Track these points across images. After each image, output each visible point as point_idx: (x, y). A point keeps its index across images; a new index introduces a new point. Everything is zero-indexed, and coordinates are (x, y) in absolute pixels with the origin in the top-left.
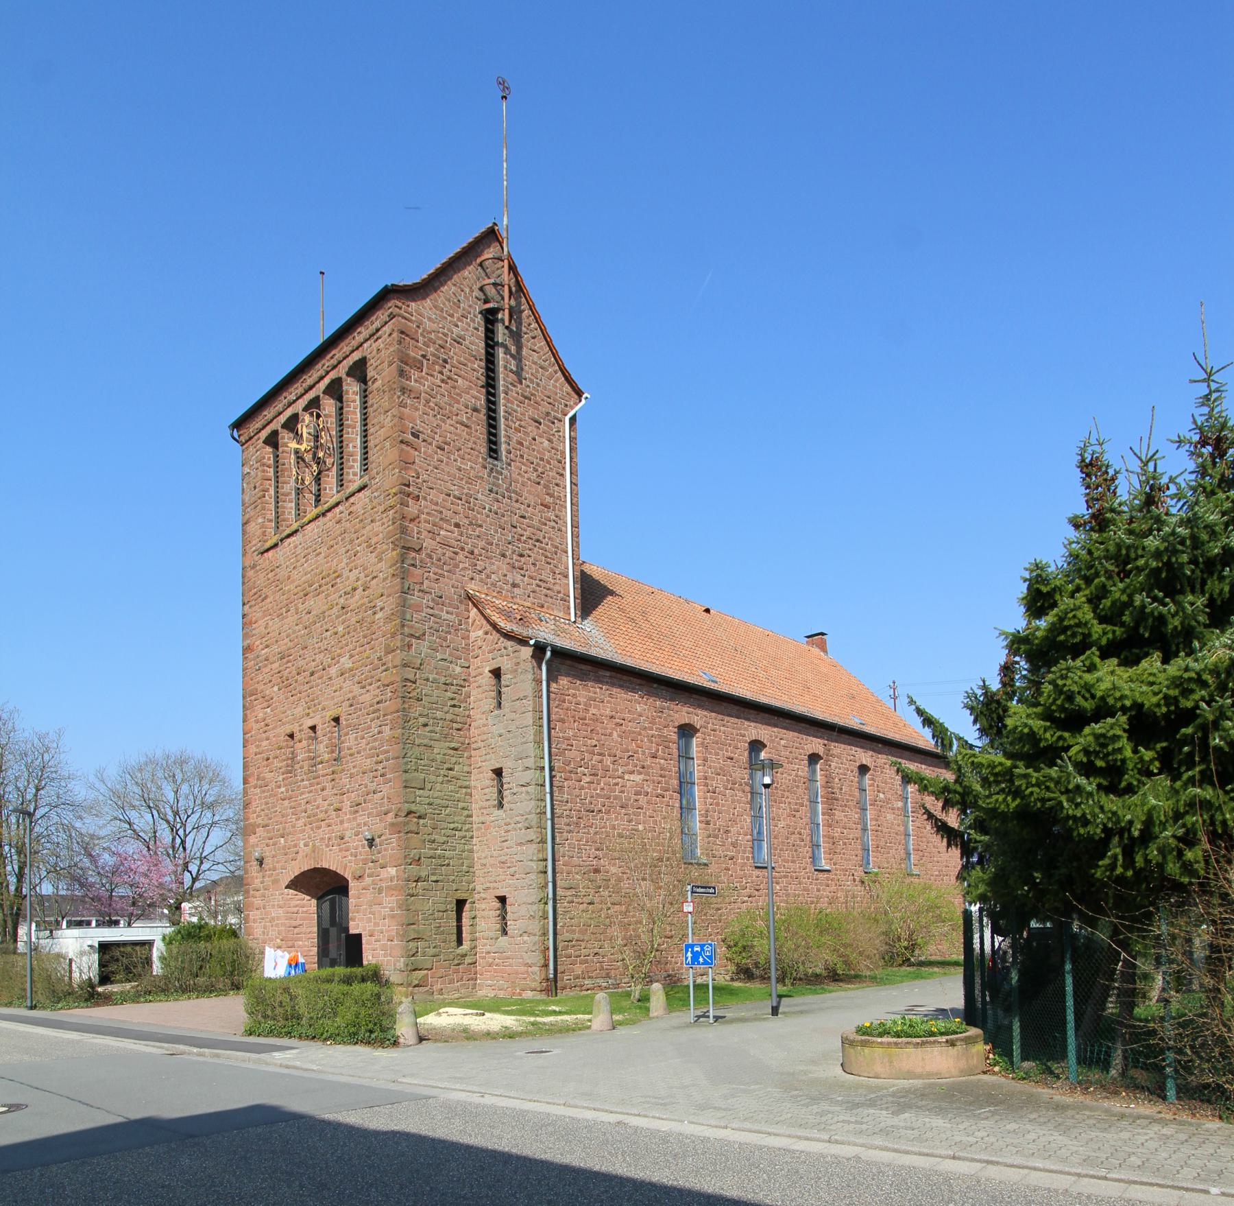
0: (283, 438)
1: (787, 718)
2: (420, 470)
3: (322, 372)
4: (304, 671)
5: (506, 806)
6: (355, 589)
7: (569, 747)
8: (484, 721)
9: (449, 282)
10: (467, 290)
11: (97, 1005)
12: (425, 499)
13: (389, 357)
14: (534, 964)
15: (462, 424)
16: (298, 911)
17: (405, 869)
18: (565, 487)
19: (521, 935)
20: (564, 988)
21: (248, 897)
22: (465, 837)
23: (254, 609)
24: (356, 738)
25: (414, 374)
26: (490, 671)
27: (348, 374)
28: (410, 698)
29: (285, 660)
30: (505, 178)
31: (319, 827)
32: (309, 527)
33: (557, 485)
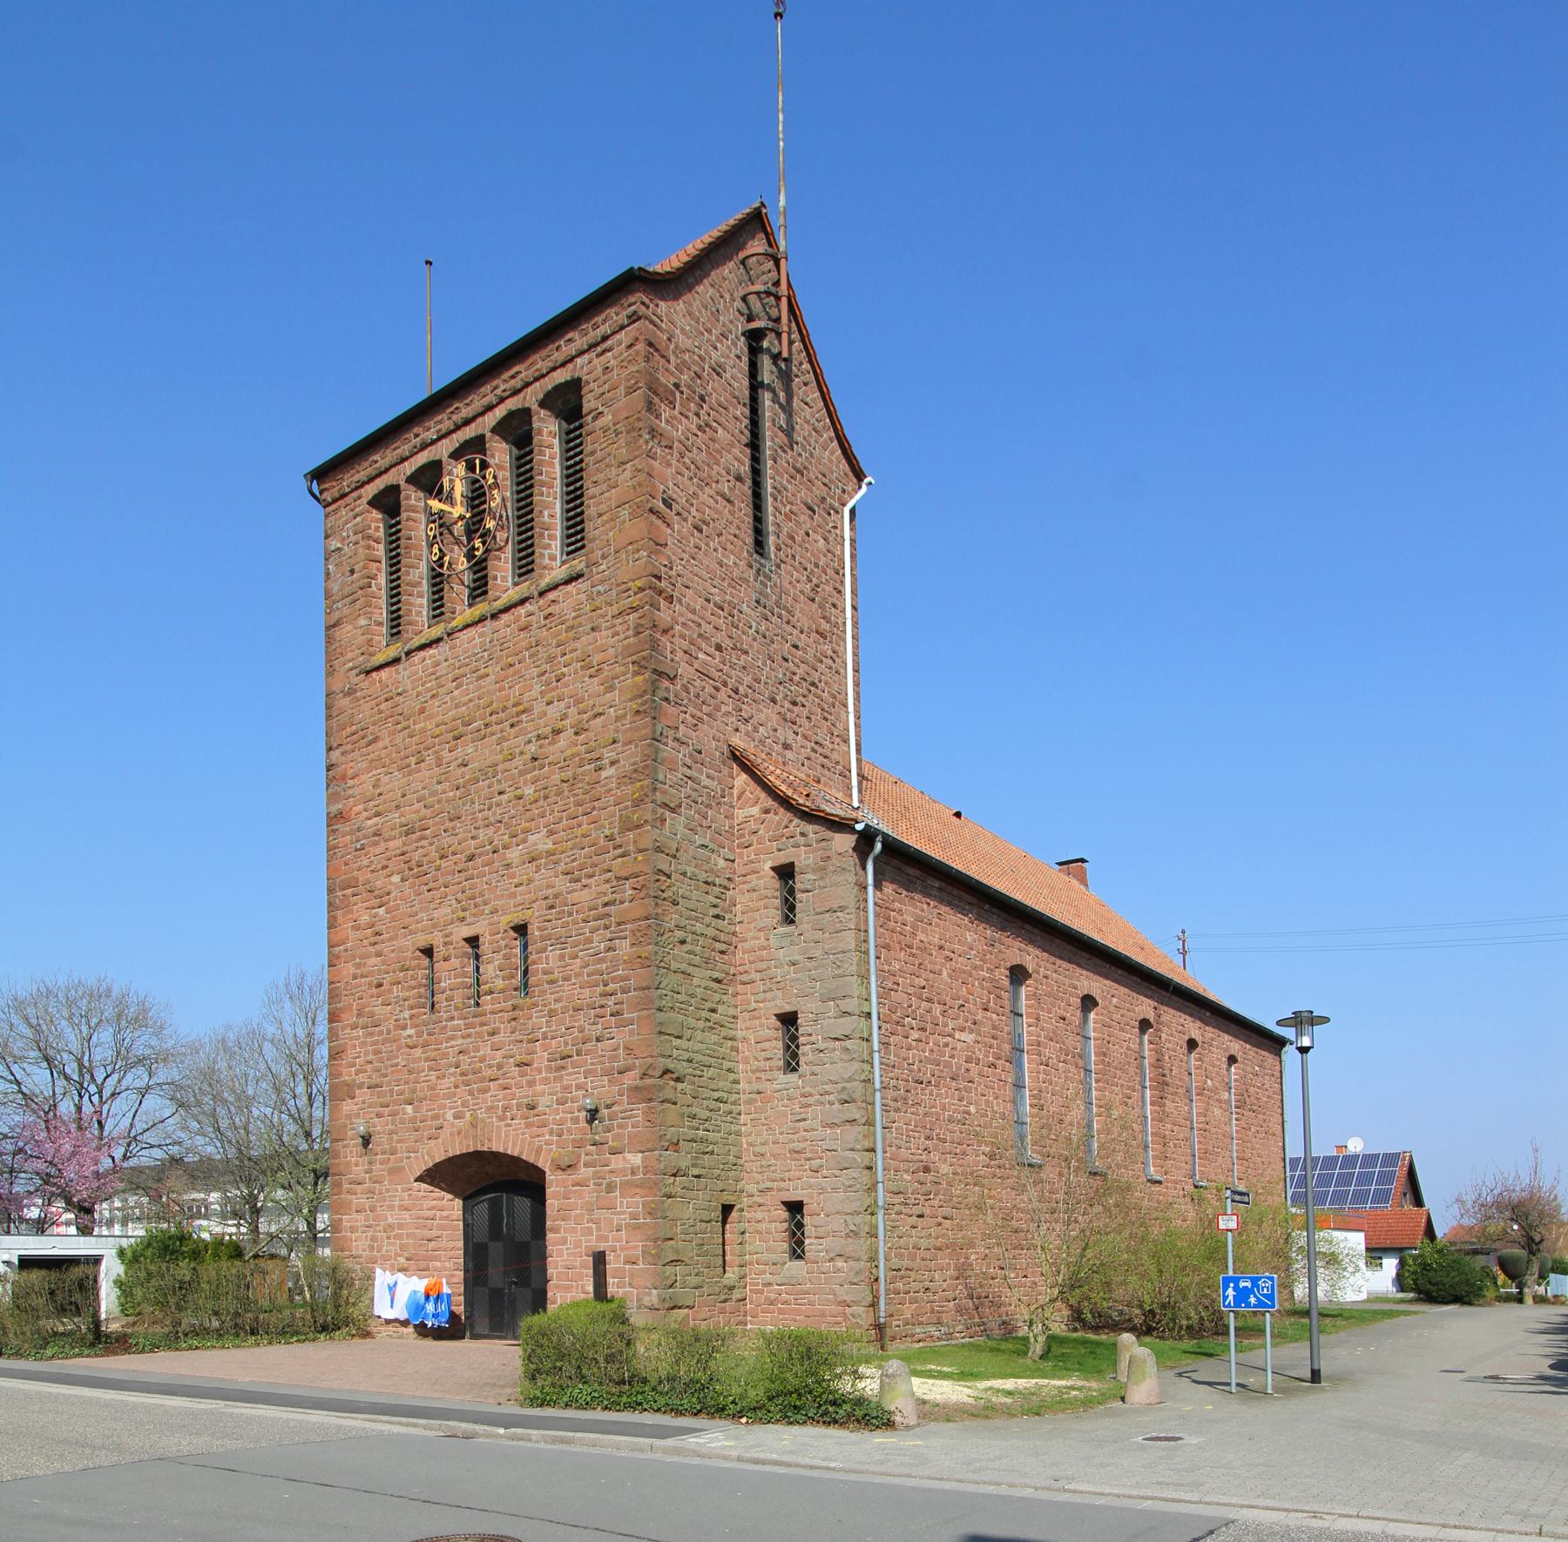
0: (408, 498)
1: (1120, 968)
2: (673, 558)
3: (491, 399)
4: (454, 854)
5: (803, 1068)
6: (557, 732)
7: (895, 987)
8: (762, 942)
9: (705, 281)
10: (727, 297)
11: (109, 1352)
12: (680, 601)
13: (628, 380)
14: (856, 1303)
15: (723, 496)
16: (435, 1215)
17: (660, 1156)
18: (843, 611)
19: (831, 1260)
20: (893, 1339)
21: (339, 1194)
22: (731, 1113)
23: (350, 756)
24: (562, 957)
25: (666, 412)
26: (773, 869)
27: (542, 404)
28: (664, 899)
29: (414, 836)
30: (781, 136)
31: (486, 1090)
32: (464, 636)
33: (834, 606)
